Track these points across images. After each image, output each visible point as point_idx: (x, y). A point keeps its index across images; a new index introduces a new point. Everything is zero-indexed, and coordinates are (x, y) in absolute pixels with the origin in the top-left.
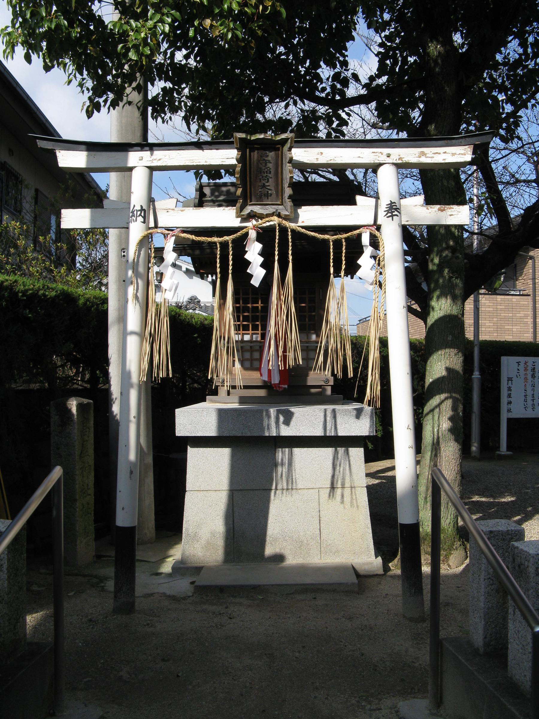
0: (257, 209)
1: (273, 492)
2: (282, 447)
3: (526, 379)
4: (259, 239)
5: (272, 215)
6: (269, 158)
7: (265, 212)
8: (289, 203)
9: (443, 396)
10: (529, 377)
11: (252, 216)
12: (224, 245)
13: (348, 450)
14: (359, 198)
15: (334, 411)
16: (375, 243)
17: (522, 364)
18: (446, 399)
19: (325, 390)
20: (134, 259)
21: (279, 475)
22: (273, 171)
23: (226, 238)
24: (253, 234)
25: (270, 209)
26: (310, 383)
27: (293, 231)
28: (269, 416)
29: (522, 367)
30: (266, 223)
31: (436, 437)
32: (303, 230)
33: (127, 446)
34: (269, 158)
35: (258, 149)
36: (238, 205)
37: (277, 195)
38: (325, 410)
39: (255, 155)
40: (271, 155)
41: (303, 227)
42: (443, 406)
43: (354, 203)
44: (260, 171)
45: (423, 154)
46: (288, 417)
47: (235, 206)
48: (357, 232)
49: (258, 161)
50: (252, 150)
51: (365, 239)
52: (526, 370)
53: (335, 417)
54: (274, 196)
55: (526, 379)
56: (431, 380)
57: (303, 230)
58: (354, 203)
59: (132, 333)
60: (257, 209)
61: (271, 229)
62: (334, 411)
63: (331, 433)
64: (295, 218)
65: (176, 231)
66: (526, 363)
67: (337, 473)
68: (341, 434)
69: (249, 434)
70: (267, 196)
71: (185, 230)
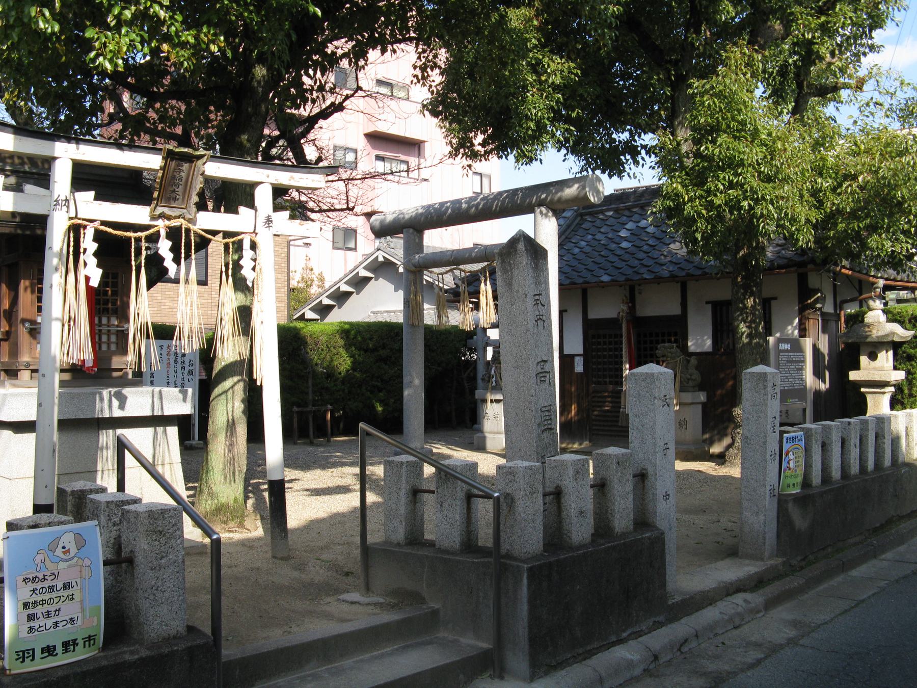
0: (166, 211)
1: (99, 474)
2: (107, 428)
3: (168, 364)
4: (169, 236)
5: (179, 217)
6: (184, 168)
7: (173, 214)
8: (194, 209)
9: (236, 379)
10: (172, 362)
11: (162, 216)
12: (138, 240)
13: (165, 430)
14: (242, 209)
15: (160, 392)
16: (253, 246)
17: (165, 348)
18: (239, 381)
19: (127, 374)
20: (61, 250)
21: (105, 457)
22: (184, 179)
23: (139, 234)
24: (163, 233)
25: (176, 212)
26: (114, 366)
27: (195, 233)
28: (102, 399)
29: (164, 352)
30: (174, 223)
31: (230, 418)
32: (203, 233)
33: (194, 425)
34: (184, 168)
35: (176, 159)
36: (153, 205)
37: (183, 198)
38: (110, 392)
39: (173, 163)
40: (186, 166)
41: (203, 230)
42: (236, 387)
43: (236, 212)
44: (174, 177)
45: (292, 178)
46: (122, 400)
47: (149, 205)
48: (239, 237)
49: (175, 169)
50: (172, 160)
51: (246, 245)
52: (169, 354)
53: (161, 398)
54: (180, 200)
55: (168, 364)
56: (223, 364)
57: (203, 233)
58: (236, 212)
59: (57, 319)
60: (166, 211)
61: (179, 228)
62: (160, 392)
63: (158, 413)
64: (192, 221)
65: (96, 224)
66: (169, 347)
67: (157, 451)
68: (166, 413)
69: (82, 417)
70: (175, 199)
71: (103, 223)
